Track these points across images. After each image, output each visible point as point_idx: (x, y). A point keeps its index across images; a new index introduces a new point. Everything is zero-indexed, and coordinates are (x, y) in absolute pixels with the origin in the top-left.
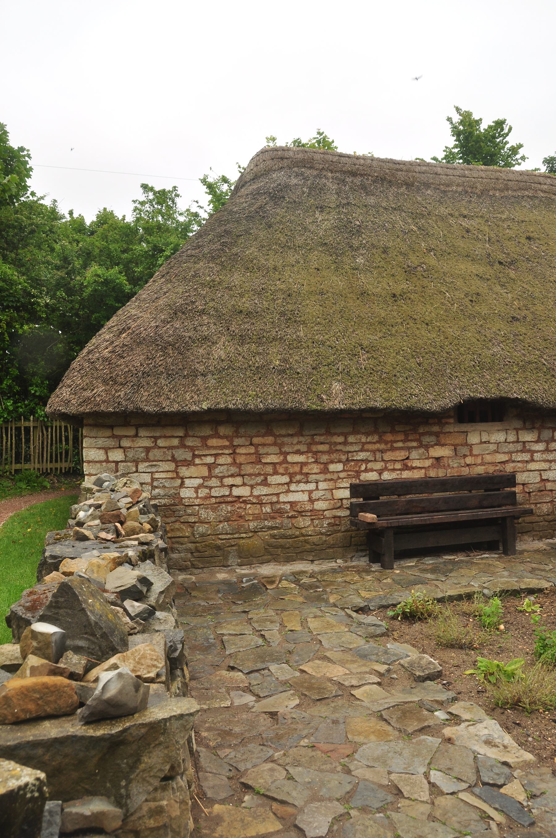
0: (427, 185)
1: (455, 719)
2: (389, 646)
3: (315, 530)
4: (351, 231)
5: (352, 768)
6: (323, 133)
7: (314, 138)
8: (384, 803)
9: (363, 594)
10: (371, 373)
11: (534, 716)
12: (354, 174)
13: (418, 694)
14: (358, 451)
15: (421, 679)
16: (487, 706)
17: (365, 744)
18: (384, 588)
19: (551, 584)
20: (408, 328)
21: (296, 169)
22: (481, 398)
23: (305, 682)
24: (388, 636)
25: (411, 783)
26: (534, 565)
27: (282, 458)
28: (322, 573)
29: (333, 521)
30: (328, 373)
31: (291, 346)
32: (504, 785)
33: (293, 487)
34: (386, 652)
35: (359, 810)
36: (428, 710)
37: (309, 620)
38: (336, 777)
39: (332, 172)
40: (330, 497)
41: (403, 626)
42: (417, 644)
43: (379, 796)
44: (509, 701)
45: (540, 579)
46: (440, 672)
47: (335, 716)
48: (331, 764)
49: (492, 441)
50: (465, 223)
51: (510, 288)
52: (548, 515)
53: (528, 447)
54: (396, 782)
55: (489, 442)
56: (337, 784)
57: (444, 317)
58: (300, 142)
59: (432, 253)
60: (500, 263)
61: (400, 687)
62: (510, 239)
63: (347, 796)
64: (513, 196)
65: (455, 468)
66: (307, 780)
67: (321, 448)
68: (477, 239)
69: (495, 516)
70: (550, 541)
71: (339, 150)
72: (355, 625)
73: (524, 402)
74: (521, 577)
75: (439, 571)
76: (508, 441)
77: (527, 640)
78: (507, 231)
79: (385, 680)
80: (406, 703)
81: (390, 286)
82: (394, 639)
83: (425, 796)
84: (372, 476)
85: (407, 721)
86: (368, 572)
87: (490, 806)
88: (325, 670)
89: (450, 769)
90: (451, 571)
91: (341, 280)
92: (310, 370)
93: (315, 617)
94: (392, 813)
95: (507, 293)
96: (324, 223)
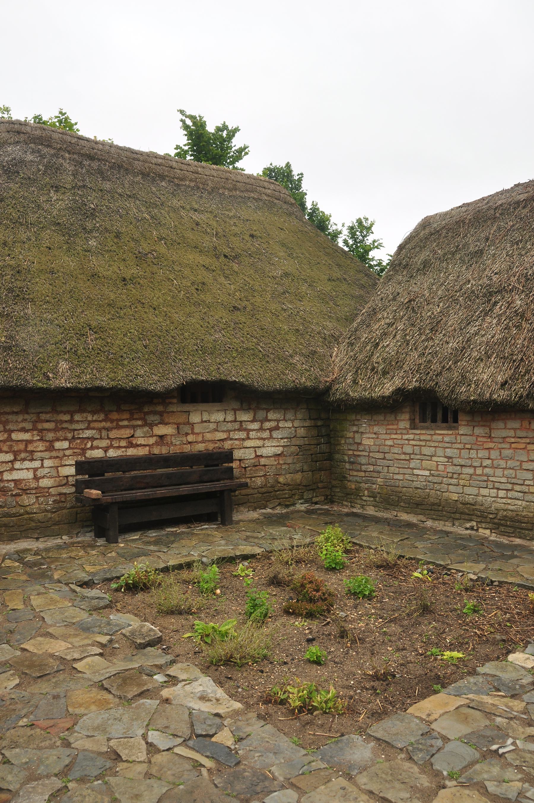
0: (162, 177)
1: (173, 680)
2: (111, 617)
3: (40, 508)
4: (85, 213)
5: (71, 740)
6: (65, 113)
7: (56, 117)
8: (103, 769)
9: (88, 568)
10: (98, 354)
11: (243, 669)
12: (91, 158)
13: (139, 660)
14: (84, 429)
15: (142, 646)
16: (202, 665)
17: (86, 715)
18: (109, 561)
19: (262, 550)
20: (136, 312)
21: (32, 145)
22: (203, 380)
23: (26, 661)
24: (111, 608)
25: (130, 746)
26: (248, 534)
27: (6, 436)
28: (47, 550)
29: (58, 498)
30: (56, 352)
31: (18, 324)
32: (216, 734)
33: (17, 465)
34: (109, 624)
35: (77, 781)
36: (148, 675)
37: (32, 597)
38: (54, 752)
39: (69, 154)
40: (55, 474)
41: (126, 597)
42: (139, 613)
43: (98, 763)
44: (223, 658)
45: (253, 546)
46: (160, 638)
47: (55, 692)
48: (51, 739)
49: (212, 421)
50: (196, 217)
51: (233, 280)
52: (262, 488)
53: (244, 426)
54: (115, 747)
55: (209, 421)
56: (55, 758)
57: (171, 303)
58: (41, 119)
59: (163, 242)
60: (225, 256)
61: (121, 656)
62: (235, 235)
63: (65, 770)
64: (240, 196)
65: (178, 446)
66: (24, 761)
67: (47, 425)
68: (206, 233)
69: (214, 490)
70: (264, 511)
71: (80, 133)
72: (78, 599)
73: (241, 384)
74: (237, 545)
75: (162, 542)
76: (227, 420)
77: (240, 601)
78: (233, 228)
79: (107, 651)
80: (127, 670)
81: (120, 270)
82: (118, 610)
83: (142, 756)
84: (98, 454)
85: (127, 688)
86: (93, 546)
87: (202, 755)
88: (47, 647)
89: (167, 727)
90: (173, 542)
91: (72, 261)
92: (37, 348)
93: (39, 594)
94: (110, 778)
95: (230, 284)
96: (59, 203)
